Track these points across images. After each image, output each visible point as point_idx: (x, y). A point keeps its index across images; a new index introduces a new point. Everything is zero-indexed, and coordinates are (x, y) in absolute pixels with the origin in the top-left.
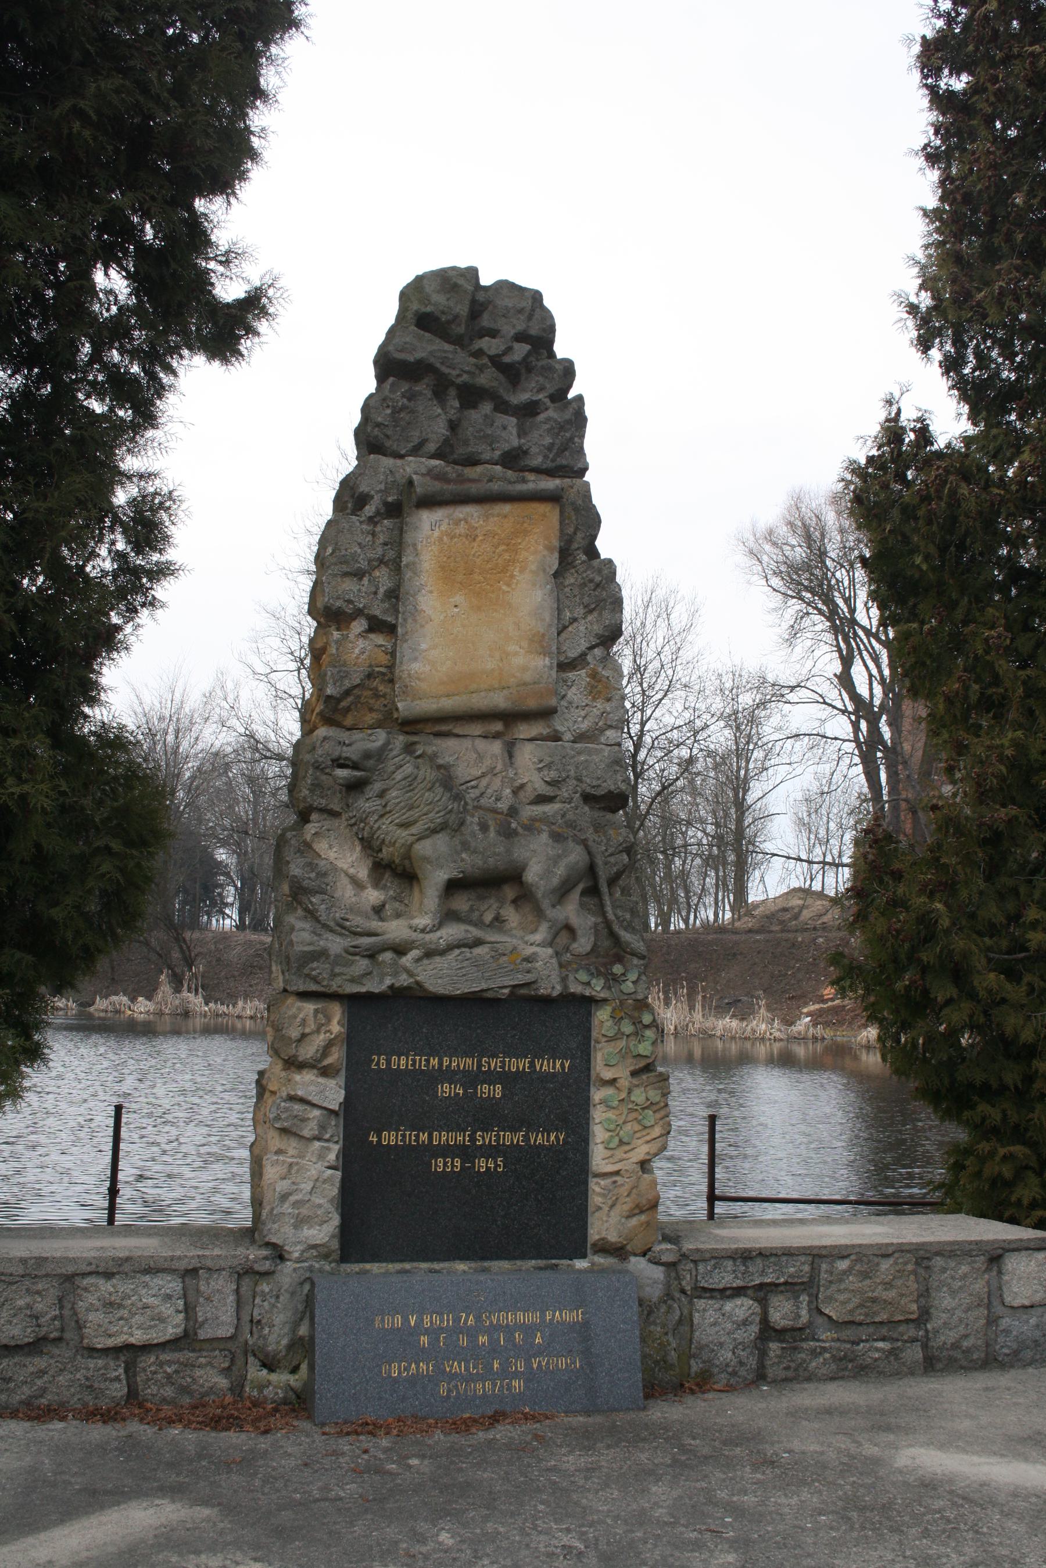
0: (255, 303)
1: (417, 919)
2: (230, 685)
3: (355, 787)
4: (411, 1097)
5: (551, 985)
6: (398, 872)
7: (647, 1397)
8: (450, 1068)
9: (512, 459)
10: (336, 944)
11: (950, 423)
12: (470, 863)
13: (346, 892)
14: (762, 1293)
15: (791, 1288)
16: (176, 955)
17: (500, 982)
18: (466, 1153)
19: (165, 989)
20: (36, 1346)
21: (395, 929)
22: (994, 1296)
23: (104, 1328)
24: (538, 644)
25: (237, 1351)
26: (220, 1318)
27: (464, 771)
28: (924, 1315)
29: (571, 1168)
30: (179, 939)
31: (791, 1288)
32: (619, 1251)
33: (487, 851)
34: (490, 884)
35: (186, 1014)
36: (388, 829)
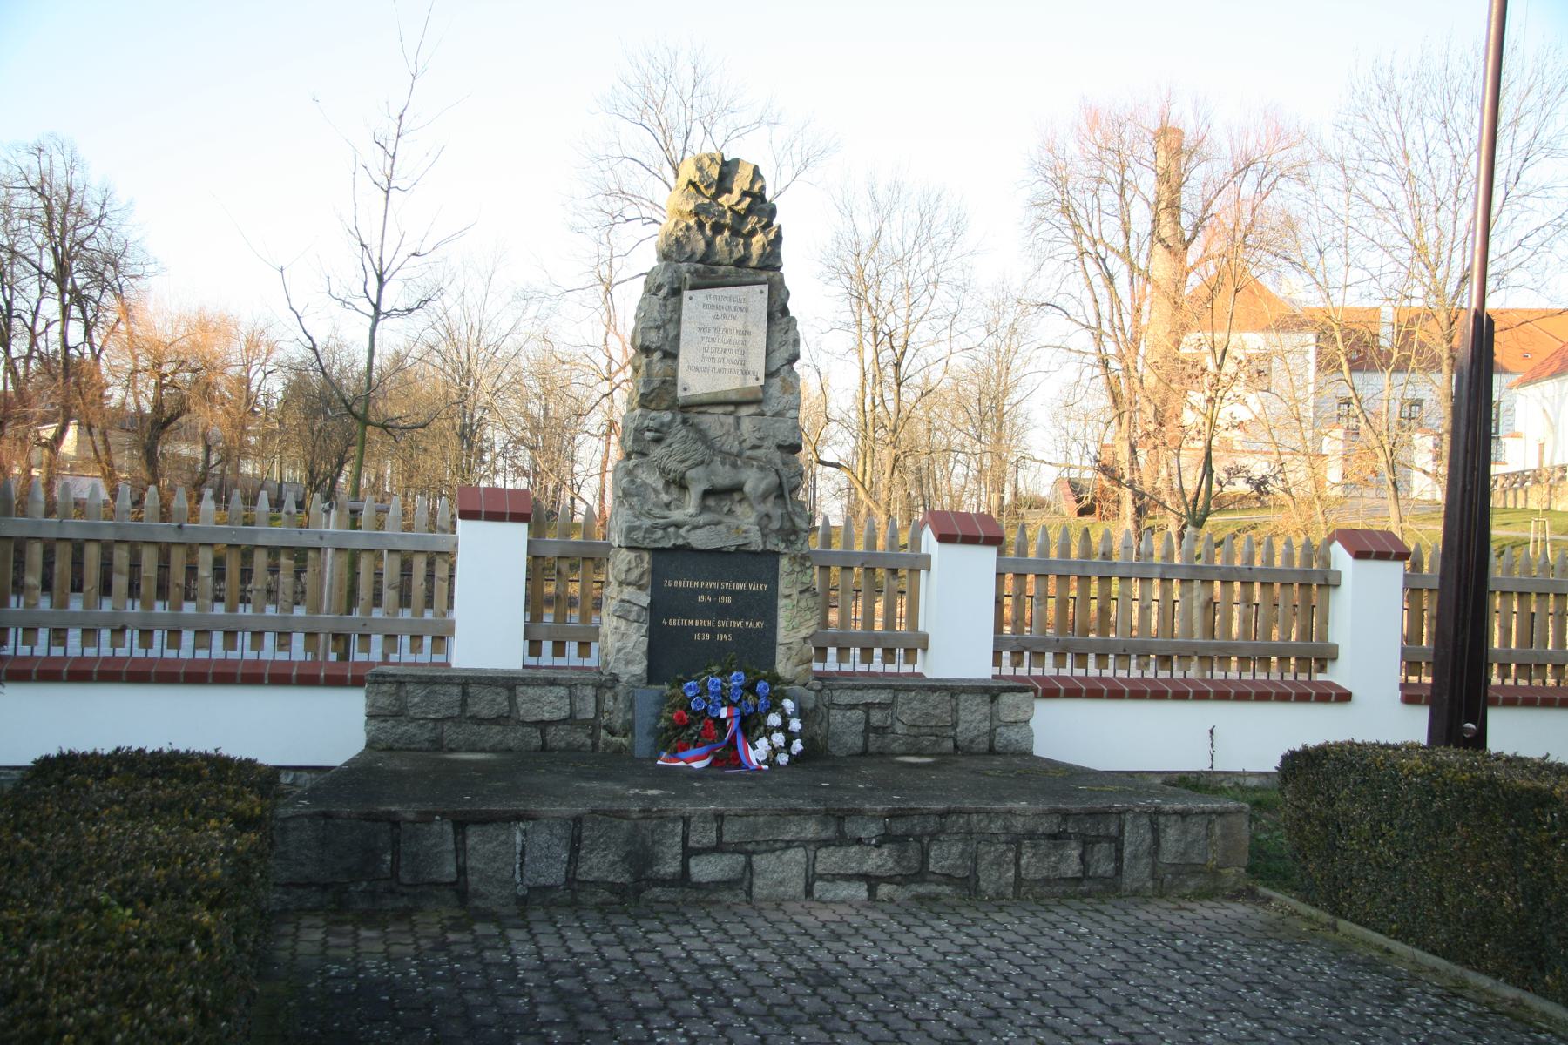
5: (756, 543)
17: (730, 542)
18: (713, 631)
20: (495, 721)
21: (676, 515)
28: (954, 725)
33: (723, 475)
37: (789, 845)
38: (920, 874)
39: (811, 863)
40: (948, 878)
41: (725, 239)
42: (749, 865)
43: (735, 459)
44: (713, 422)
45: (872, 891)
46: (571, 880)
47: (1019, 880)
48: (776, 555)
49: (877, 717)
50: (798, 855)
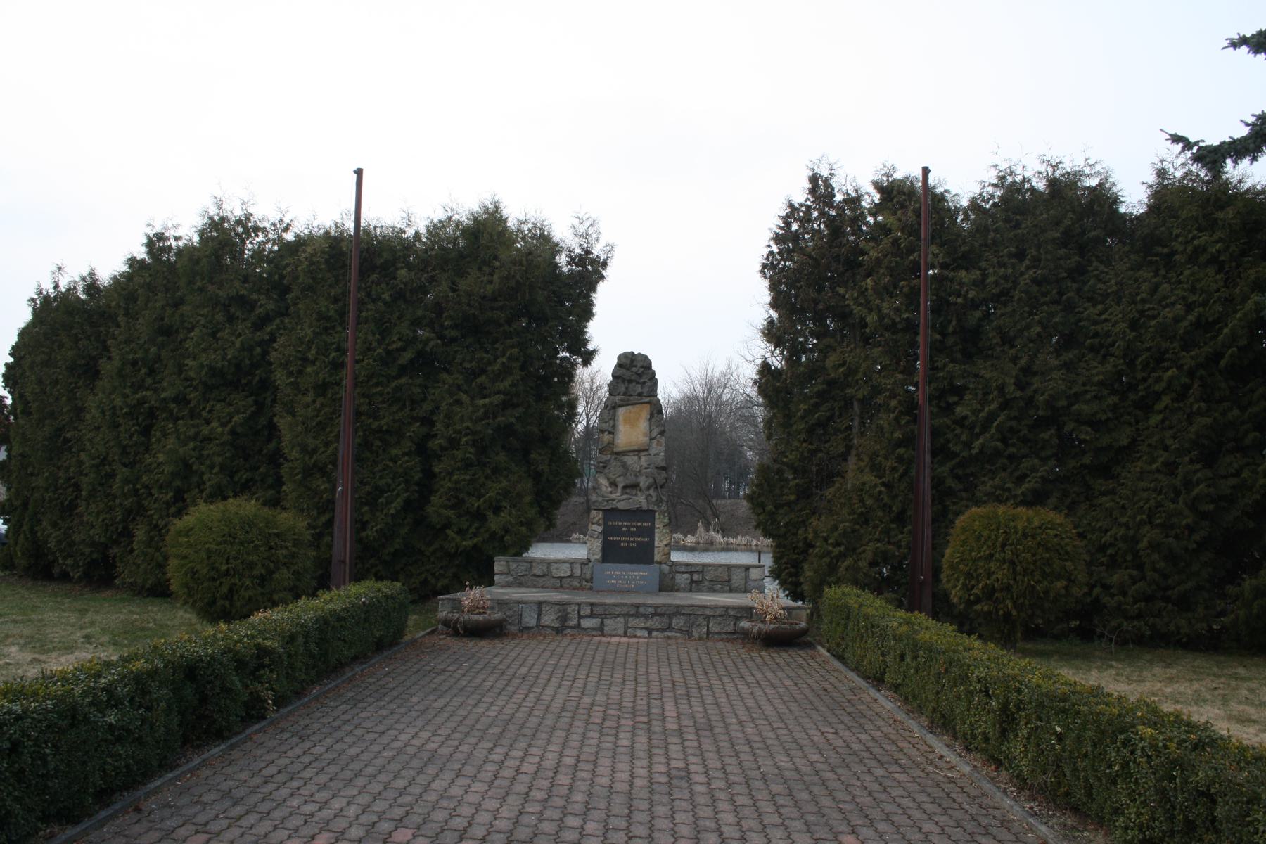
0: (593, 352)
1: (617, 494)
2: (734, 367)
3: (605, 467)
4: (617, 531)
5: (645, 507)
6: (613, 484)
7: (660, 591)
8: (624, 524)
9: (640, 394)
10: (600, 499)
11: (777, 362)
12: (628, 482)
13: (604, 489)
14: (691, 573)
15: (697, 572)
16: (709, 512)
17: (634, 507)
18: (628, 542)
19: (701, 530)
20: (543, 576)
21: (613, 496)
22: (746, 577)
23: (556, 573)
24: (645, 435)
25: (580, 578)
26: (578, 572)
27: (629, 463)
28: (729, 580)
29: (650, 546)
30: (710, 504)
31: (697, 572)
32: (660, 563)
33: (631, 480)
34: (632, 487)
35: (712, 543)
36: (610, 475)
37: (618, 615)
38: (670, 628)
39: (626, 623)
40: (679, 630)
41: (926, 171)
42: (602, 623)
43: (638, 474)
44: (630, 460)
45: (650, 633)
46: (538, 625)
47: (708, 633)
48: (654, 511)
49: (695, 577)
50: (621, 619)
